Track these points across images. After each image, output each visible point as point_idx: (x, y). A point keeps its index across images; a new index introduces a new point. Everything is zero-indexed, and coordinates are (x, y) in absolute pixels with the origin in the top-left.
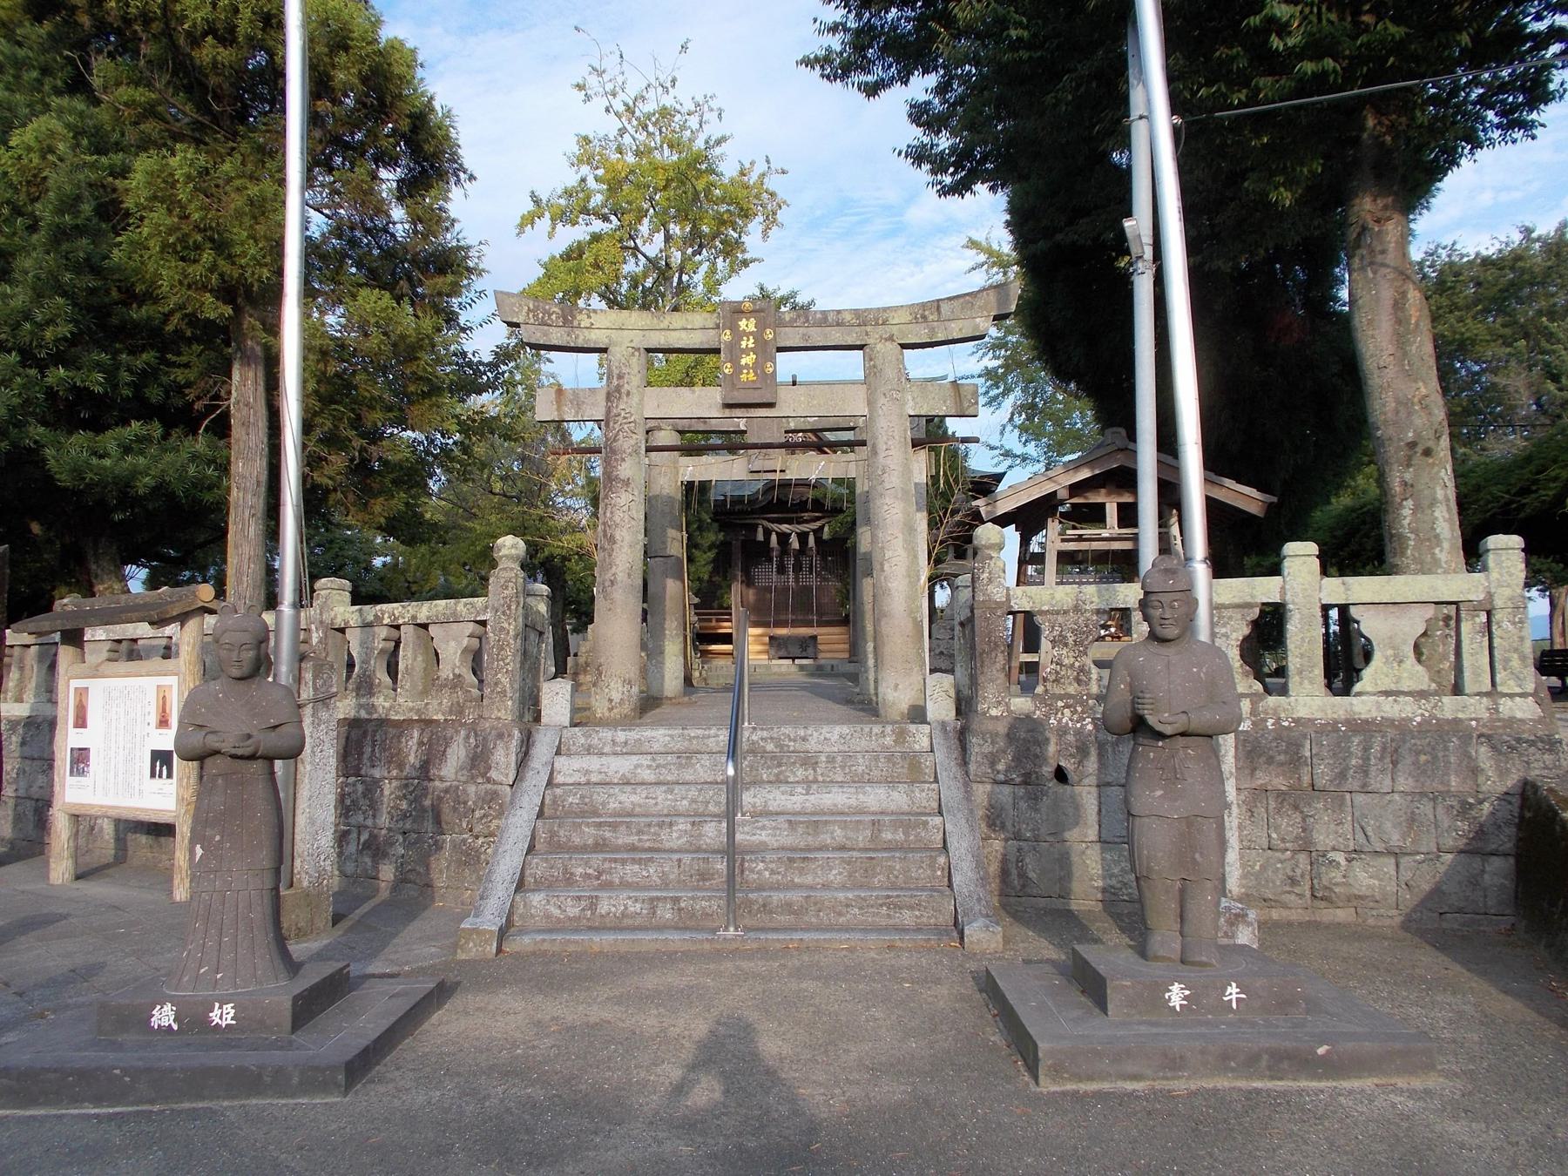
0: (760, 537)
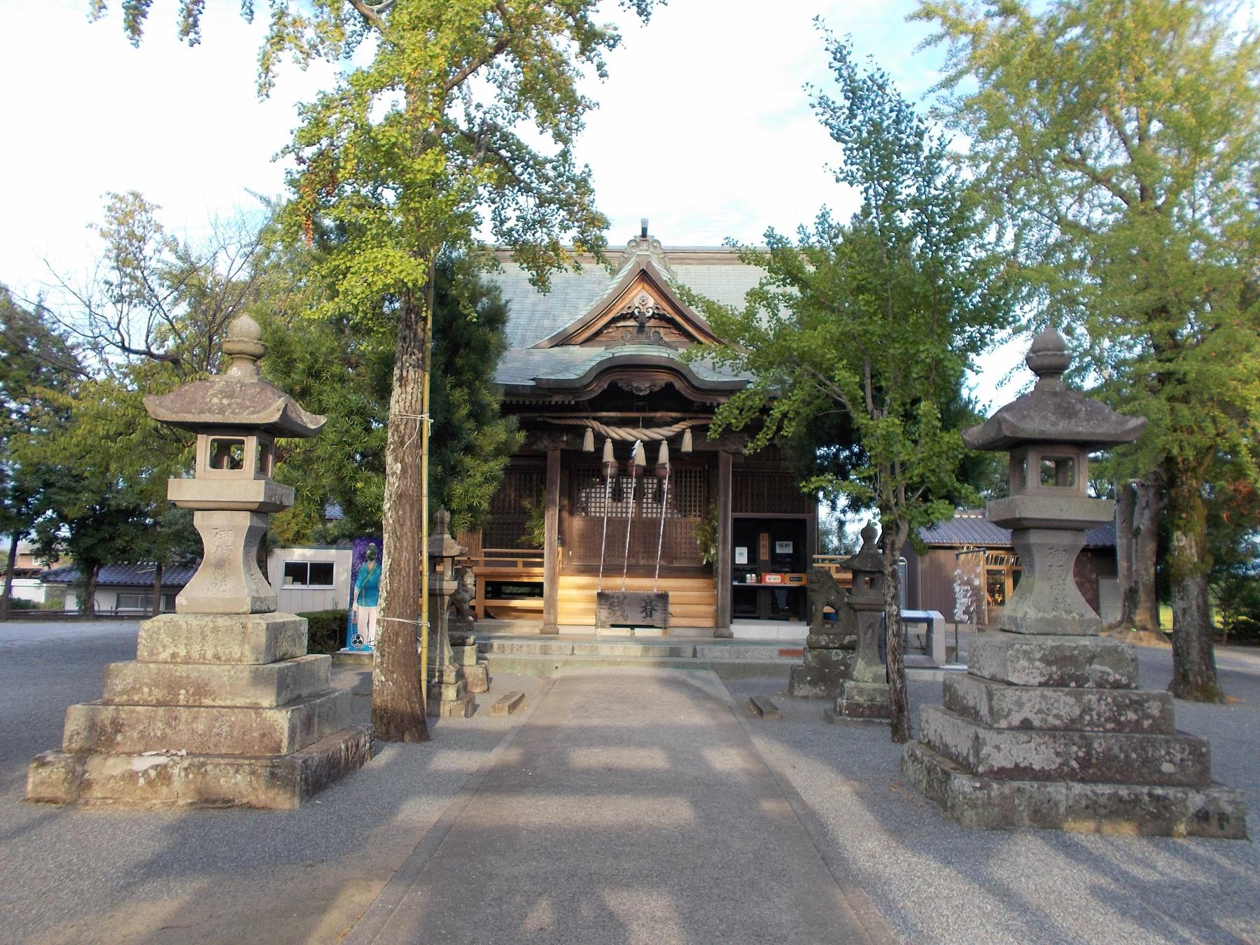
0: (589, 445)
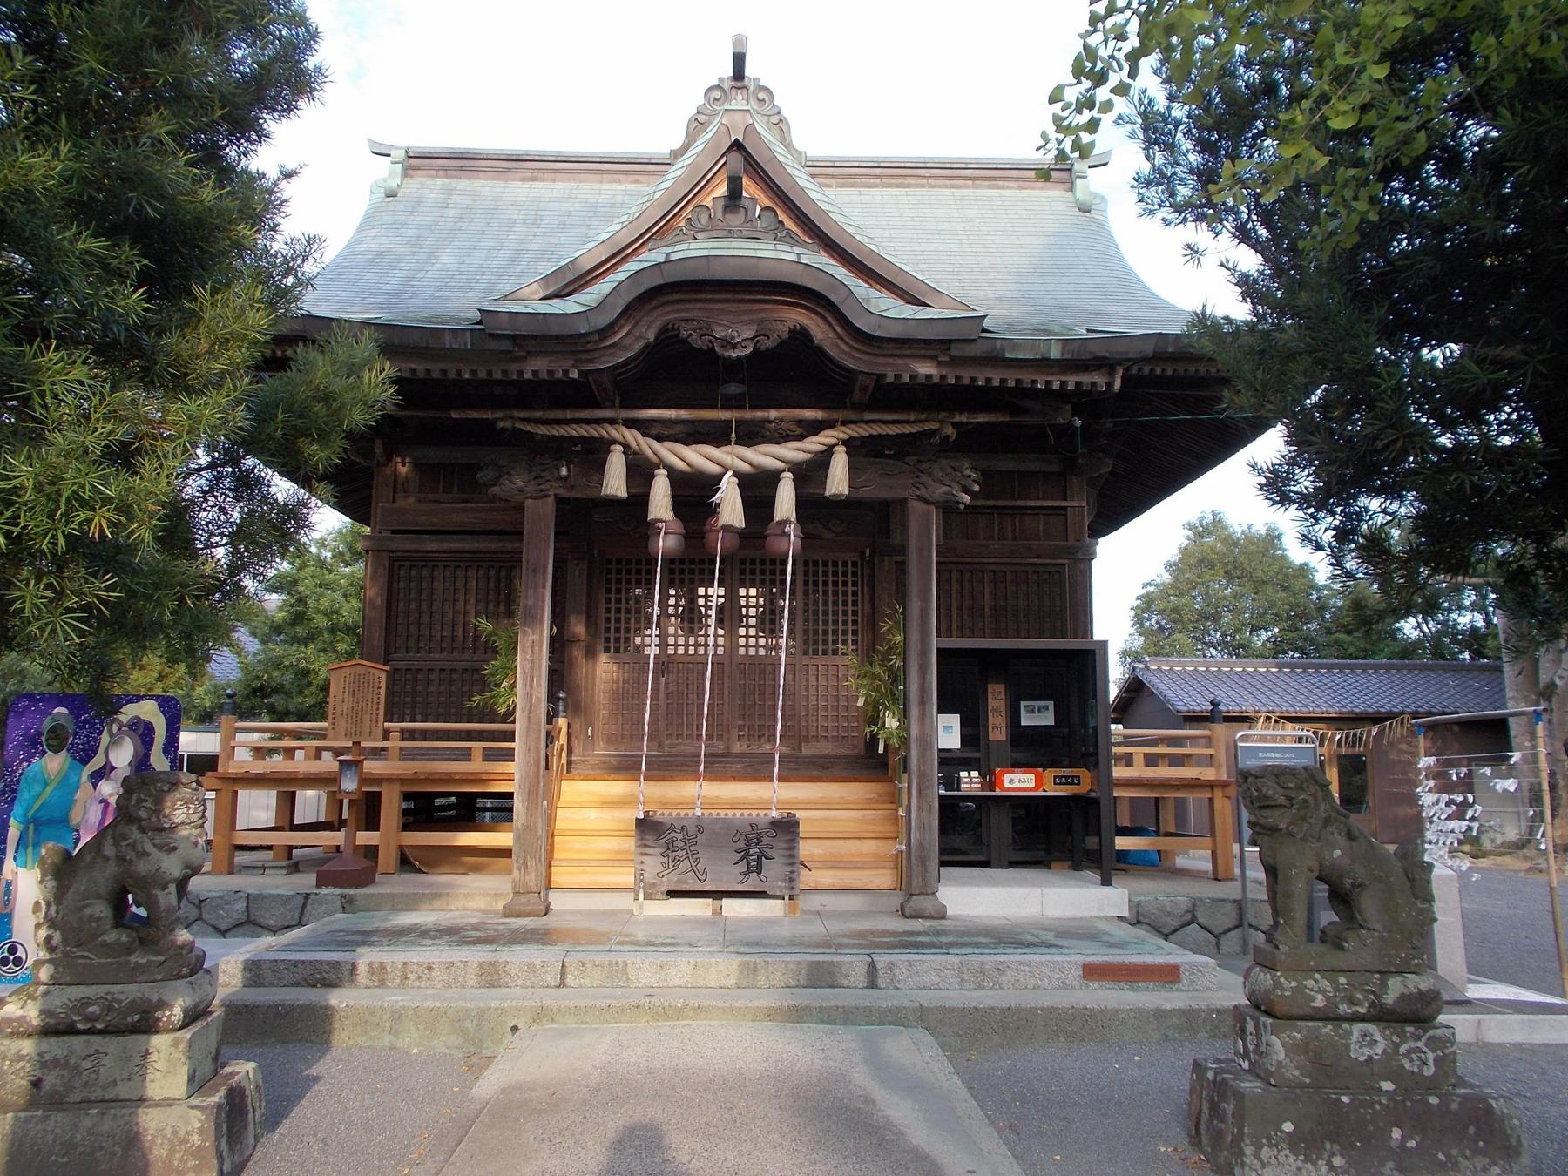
0: (615, 482)
